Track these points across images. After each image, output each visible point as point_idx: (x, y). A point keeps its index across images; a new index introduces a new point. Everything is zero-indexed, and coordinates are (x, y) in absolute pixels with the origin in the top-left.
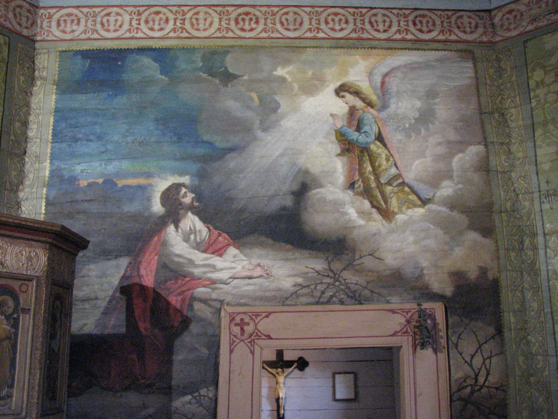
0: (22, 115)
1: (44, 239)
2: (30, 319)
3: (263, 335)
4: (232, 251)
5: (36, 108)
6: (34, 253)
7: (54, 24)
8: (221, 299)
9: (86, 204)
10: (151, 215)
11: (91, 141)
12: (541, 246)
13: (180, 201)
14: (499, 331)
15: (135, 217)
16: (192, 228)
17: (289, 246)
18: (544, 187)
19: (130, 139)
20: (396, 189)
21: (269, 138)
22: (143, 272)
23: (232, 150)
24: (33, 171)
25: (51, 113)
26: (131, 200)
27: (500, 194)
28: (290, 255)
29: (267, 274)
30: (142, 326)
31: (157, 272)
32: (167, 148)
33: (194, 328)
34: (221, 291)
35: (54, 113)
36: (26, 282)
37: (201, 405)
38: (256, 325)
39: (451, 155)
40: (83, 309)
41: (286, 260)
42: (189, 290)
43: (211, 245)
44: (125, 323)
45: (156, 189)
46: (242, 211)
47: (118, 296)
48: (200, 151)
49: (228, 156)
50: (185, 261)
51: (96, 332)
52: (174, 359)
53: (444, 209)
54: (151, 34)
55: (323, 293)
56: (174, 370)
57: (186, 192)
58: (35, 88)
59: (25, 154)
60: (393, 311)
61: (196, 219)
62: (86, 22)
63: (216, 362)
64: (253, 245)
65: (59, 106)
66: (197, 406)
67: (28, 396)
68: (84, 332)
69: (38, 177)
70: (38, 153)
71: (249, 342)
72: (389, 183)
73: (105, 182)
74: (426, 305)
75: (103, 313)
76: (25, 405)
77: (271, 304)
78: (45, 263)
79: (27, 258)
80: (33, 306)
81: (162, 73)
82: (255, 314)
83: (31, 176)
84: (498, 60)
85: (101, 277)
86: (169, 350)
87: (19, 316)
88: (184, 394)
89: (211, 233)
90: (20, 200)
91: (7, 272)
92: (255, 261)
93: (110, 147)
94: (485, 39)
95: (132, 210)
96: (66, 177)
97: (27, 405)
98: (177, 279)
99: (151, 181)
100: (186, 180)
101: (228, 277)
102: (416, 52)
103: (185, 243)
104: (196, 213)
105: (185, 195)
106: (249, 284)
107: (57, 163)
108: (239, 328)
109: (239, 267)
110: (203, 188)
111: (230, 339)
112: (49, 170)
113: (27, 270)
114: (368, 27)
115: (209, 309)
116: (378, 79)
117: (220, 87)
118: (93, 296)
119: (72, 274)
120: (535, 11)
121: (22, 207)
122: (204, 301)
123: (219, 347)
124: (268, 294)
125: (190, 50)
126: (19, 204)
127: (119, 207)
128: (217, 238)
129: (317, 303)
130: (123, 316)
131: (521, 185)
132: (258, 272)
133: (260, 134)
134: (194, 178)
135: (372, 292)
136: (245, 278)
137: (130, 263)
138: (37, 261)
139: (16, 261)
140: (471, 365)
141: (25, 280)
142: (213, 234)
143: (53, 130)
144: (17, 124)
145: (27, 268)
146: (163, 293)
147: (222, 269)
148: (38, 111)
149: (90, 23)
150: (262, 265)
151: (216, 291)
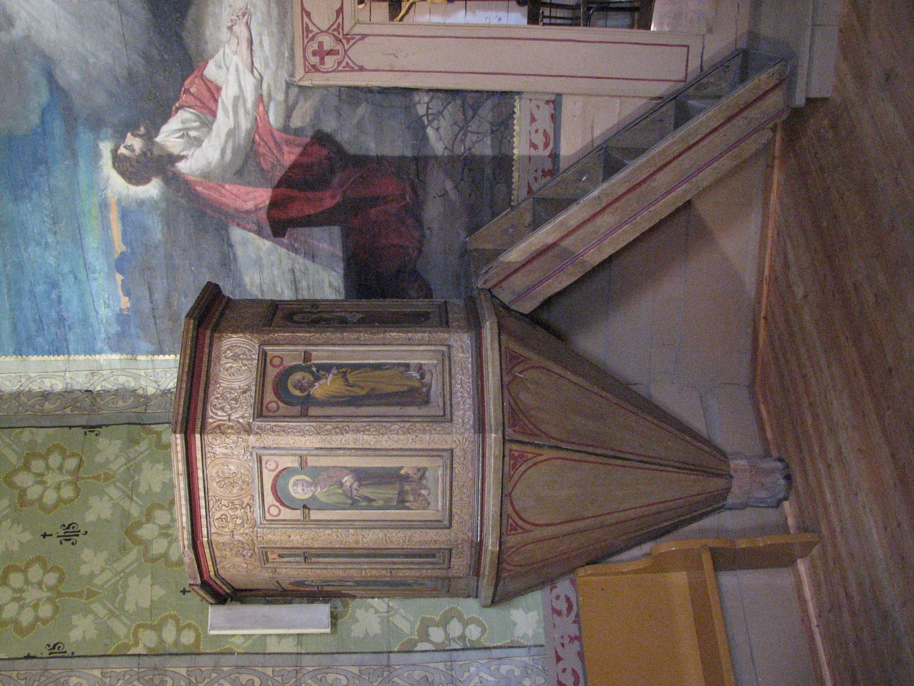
0: (33, 400)
1: (207, 341)
2: (317, 351)
3: (336, 20)
4: (211, 71)
5: (20, 384)
6: (228, 352)
8: (284, 86)
9: (158, 296)
10: (165, 197)
11: (60, 297)
13: (139, 155)
15: (169, 222)
16: (180, 134)
19: (51, 239)
21: (23, 14)
22: (250, 205)
23: (51, 78)
24: (115, 377)
25: (24, 360)
26: (145, 230)
29: (244, 15)
30: (328, 203)
31: (250, 184)
32: (59, 180)
33: (329, 125)
34: (272, 88)
35: (24, 356)
36: (268, 359)
37: (440, 113)
38: (322, 32)
40: (309, 289)
42: (272, 134)
43: (203, 103)
44: (326, 228)
45: (124, 193)
46: (147, 58)
47: (288, 239)
48: (58, 127)
49: (61, 82)
51: (340, 268)
52: (375, 154)
56: (390, 154)
57: (125, 147)
59: (91, 391)
61: (166, 129)
63: (379, 92)
64: (200, 40)
65: (11, 350)
66: (442, 119)
67: (419, 345)
68: (342, 285)
69: (123, 369)
70: (87, 372)
71: (348, 43)
73: (121, 271)
75: (313, 261)
76: (433, 348)
77: (289, 8)
78: (241, 337)
79: (235, 360)
80: (300, 348)
82: (305, 34)
83: (122, 380)
85: (261, 267)
86: (361, 161)
87: (314, 364)
88: (425, 138)
89: (186, 104)
90: (158, 391)
91: (256, 385)
92: (225, 34)
93: (66, 268)
95: (160, 227)
96: (119, 329)
97: (431, 345)
98: (257, 154)
99: (113, 200)
100: (106, 148)
101: (251, 75)
103: (204, 144)
105: (130, 148)
106: (261, 43)
107: (99, 345)
108: (327, 58)
109: (236, 59)
110: (116, 121)
111: (344, 71)
112: (111, 354)
113: (252, 359)
115: (299, 105)
118: (289, 276)
119: (255, 302)
121: (168, 388)
122: (289, 113)
123: (357, 88)
124: (275, 12)
126: (165, 393)
127: (156, 247)
128: (192, 95)
130: (316, 230)
132: (241, 29)
133: (18, 31)
134: (102, 136)
136: (252, 50)
137: (238, 225)
138: (239, 347)
139: (241, 375)
141: (265, 360)
142: (186, 102)
143: (49, 354)
144: (47, 406)
145: (248, 360)
146: (279, 174)
147: (240, 86)
148: (23, 380)
150: (230, 24)
151: (273, 95)
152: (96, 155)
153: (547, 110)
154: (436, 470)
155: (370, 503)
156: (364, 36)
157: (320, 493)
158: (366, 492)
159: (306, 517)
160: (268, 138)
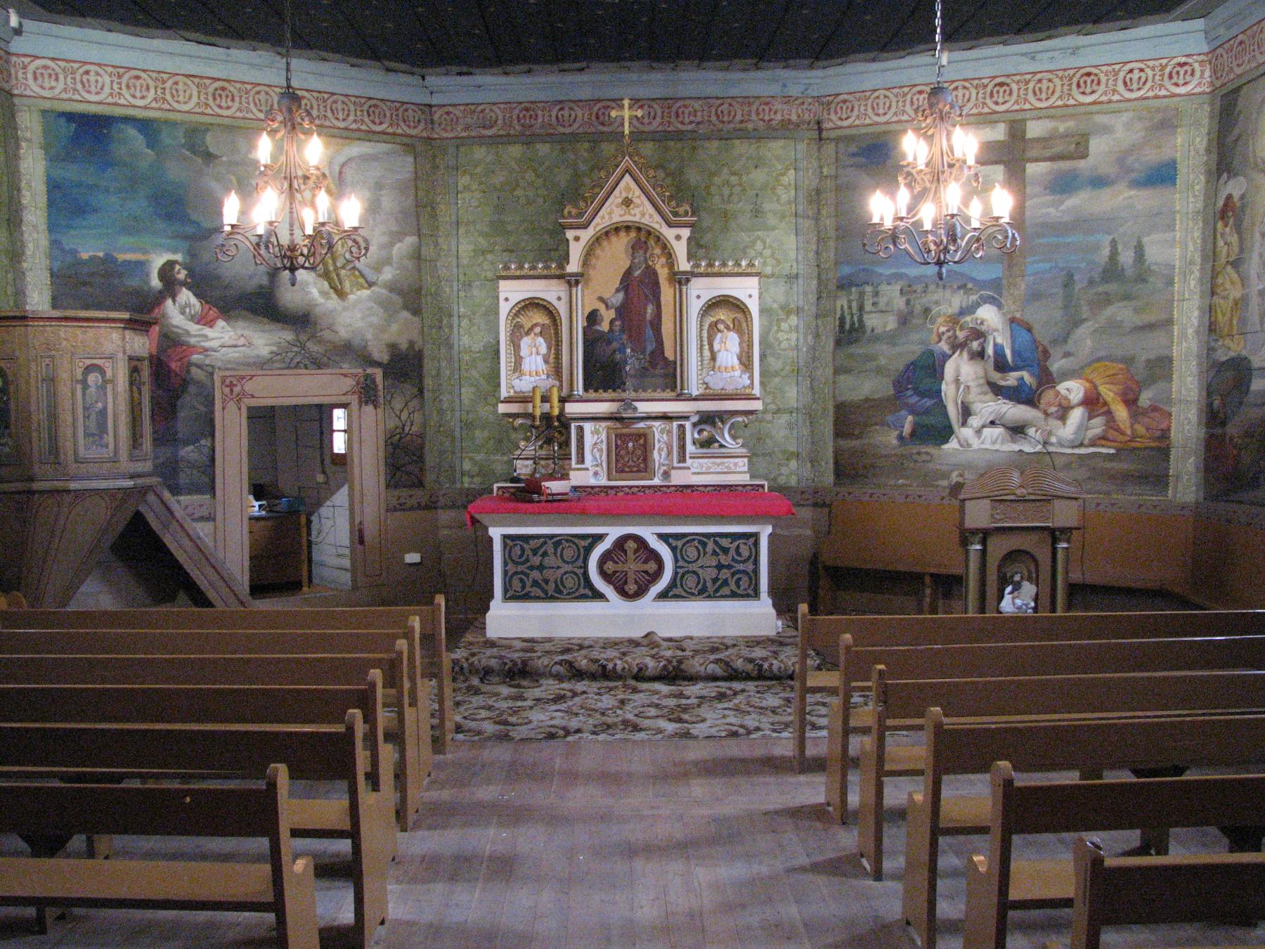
4: (221, 323)
7: (30, 76)
10: (150, 288)
12: (455, 326)
14: (421, 391)
17: (266, 320)
18: (462, 277)
20: (349, 273)
27: (428, 281)
28: (267, 327)
33: (192, 389)
39: (392, 244)
41: (263, 331)
50: (181, 331)
53: (384, 291)
54: (133, 101)
55: (292, 359)
58: (21, 151)
60: (345, 376)
61: (190, 294)
62: (65, 78)
64: (237, 318)
72: (343, 267)
74: (369, 371)
81: (148, 147)
83: (31, 246)
84: (434, 157)
88: (188, 444)
92: (240, 332)
94: (424, 134)
98: (176, 346)
100: (178, 257)
102: (368, 144)
104: (189, 289)
105: (179, 272)
109: (227, 338)
114: (329, 114)
116: (337, 169)
117: (203, 167)
120: (469, 120)
122: (199, 366)
124: (251, 360)
125: (173, 124)
129: (287, 368)
131: (443, 272)
132: (242, 341)
135: (329, 359)
140: (400, 418)
149: (69, 80)
152: (175, 251)
153: (206, 514)
154: (108, 453)
155: (87, 417)
156: (240, 409)
157: (92, 390)
158: (93, 416)
159: (77, 381)
160: (184, 354)
